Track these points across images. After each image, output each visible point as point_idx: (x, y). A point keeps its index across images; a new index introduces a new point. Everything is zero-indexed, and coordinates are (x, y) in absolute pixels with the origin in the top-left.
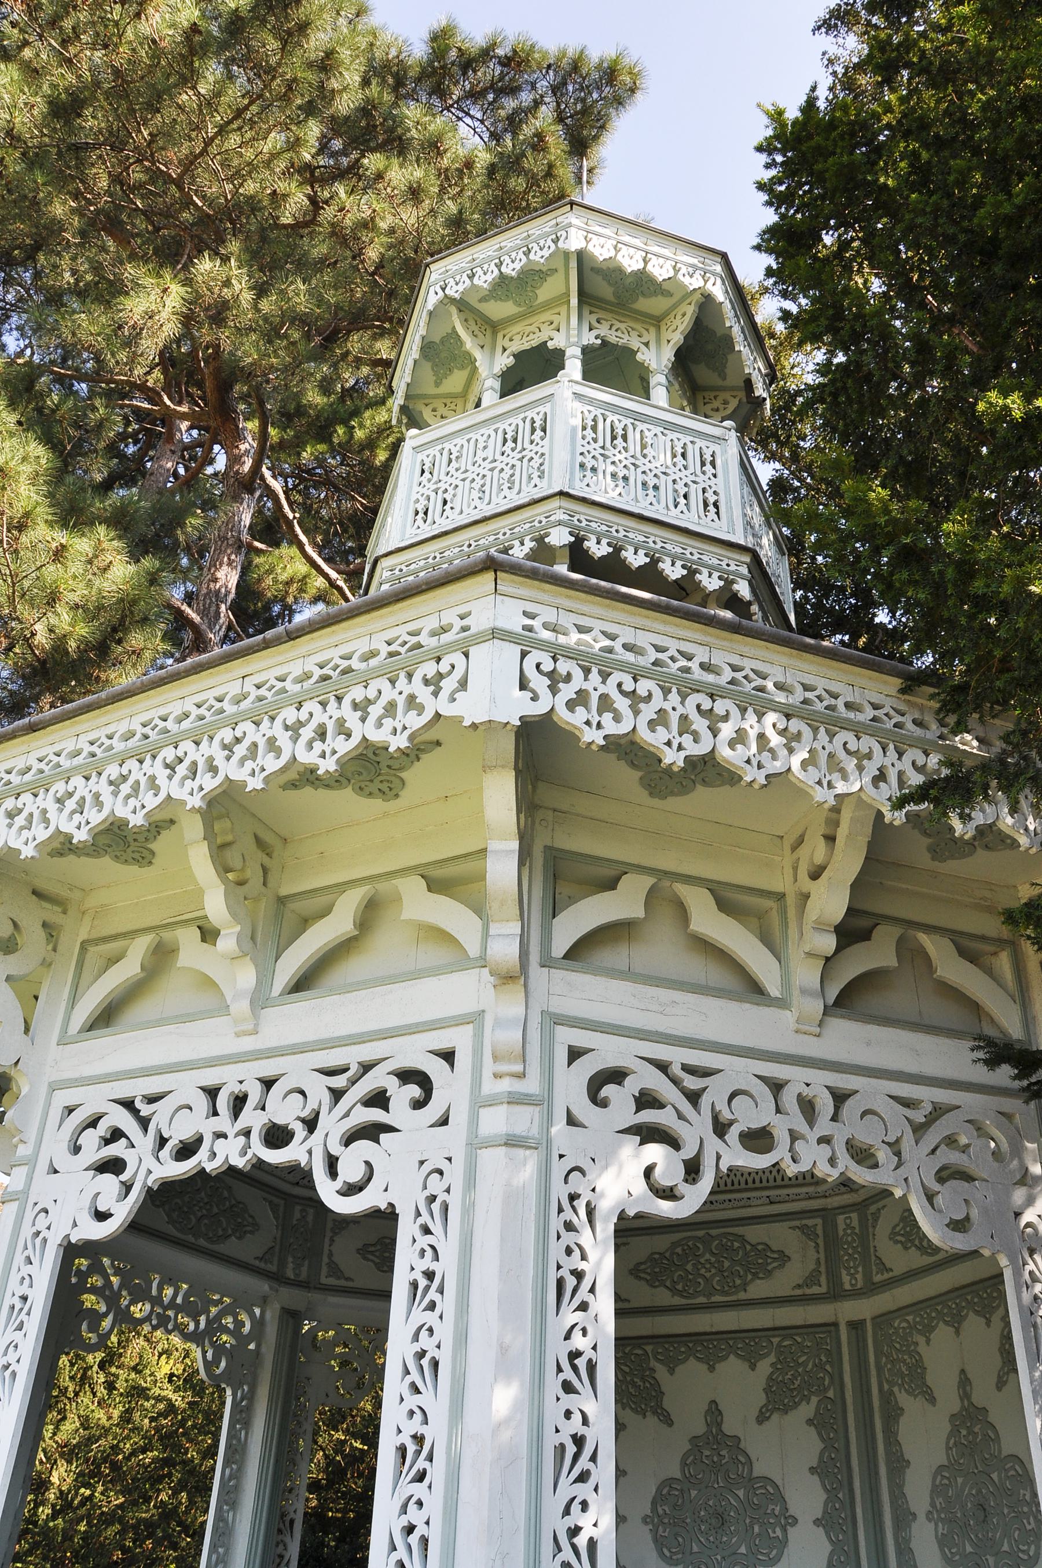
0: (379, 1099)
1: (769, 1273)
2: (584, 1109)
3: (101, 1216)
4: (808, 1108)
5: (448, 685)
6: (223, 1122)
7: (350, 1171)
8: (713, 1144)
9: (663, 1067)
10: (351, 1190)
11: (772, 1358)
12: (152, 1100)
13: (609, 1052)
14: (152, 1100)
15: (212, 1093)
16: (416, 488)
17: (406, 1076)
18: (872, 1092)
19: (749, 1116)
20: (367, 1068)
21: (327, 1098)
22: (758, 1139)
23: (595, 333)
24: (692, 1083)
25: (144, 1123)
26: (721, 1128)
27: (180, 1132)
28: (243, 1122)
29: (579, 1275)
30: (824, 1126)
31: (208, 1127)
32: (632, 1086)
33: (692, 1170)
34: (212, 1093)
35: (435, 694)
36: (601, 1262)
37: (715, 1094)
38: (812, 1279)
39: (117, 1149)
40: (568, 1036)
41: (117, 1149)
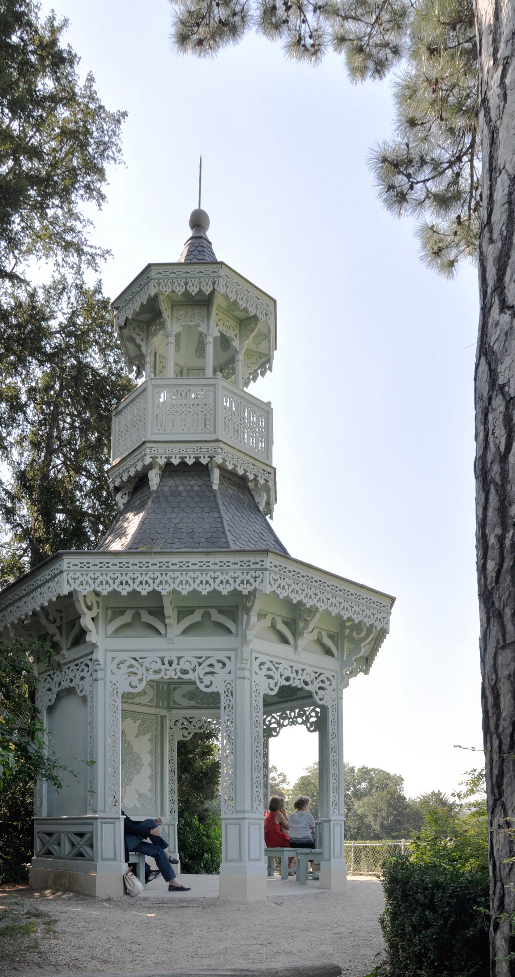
0: (211, 665)
1: (189, 692)
2: (115, 670)
4: (297, 672)
5: (259, 580)
11: (140, 721)
13: (121, 656)
17: (219, 661)
18: (309, 670)
19: (287, 674)
20: (207, 658)
22: (287, 679)
26: (148, 670)
30: (300, 676)
32: (127, 664)
33: (276, 684)
34: (162, 659)
35: (255, 581)
38: (175, 689)
40: (255, 655)
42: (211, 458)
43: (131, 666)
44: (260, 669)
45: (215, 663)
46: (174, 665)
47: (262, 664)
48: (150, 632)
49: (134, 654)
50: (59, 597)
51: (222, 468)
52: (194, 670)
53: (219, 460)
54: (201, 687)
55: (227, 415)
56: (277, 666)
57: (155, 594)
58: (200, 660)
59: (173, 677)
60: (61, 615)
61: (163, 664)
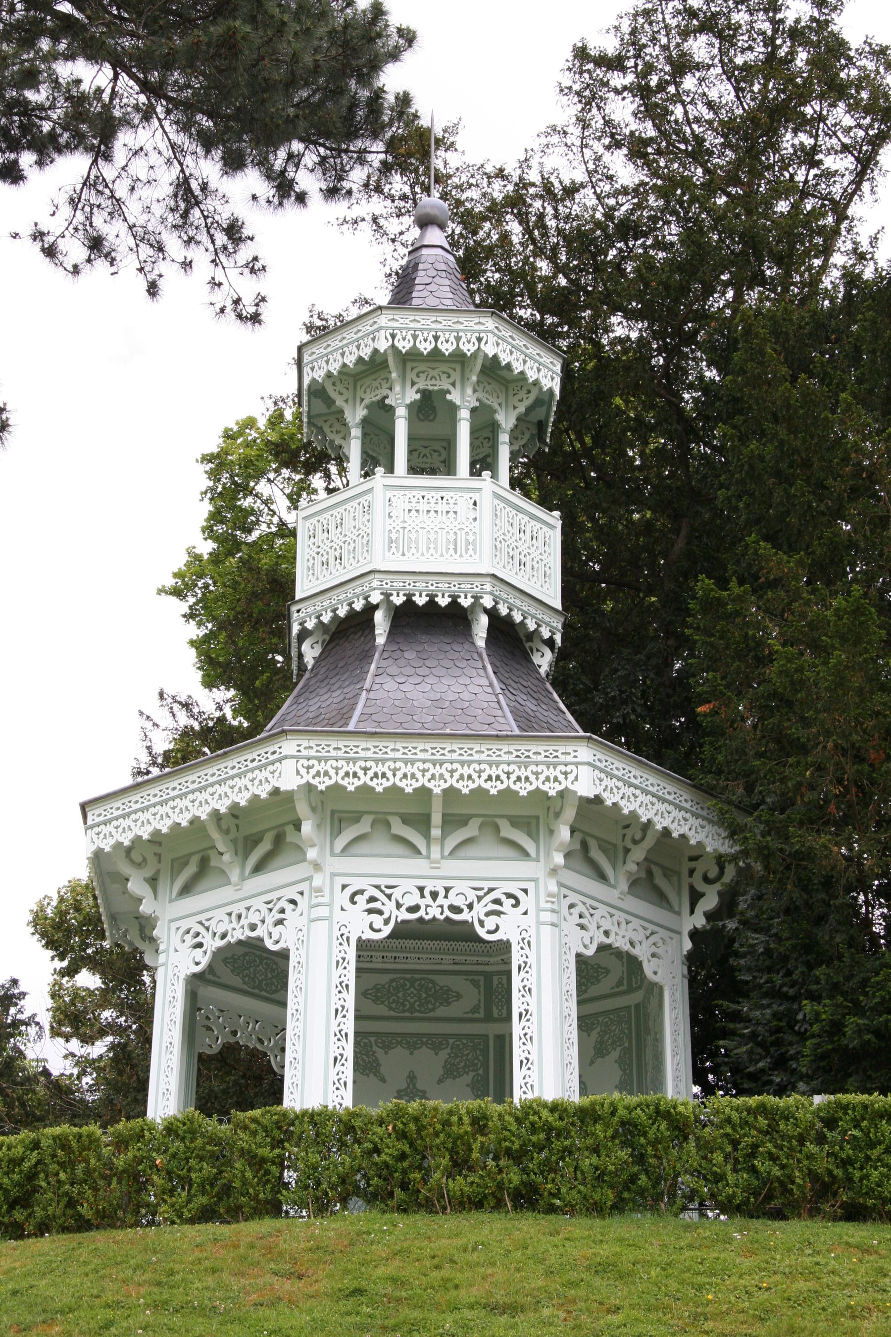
0: (497, 902)
2: (347, 905)
3: (197, 964)
4: (434, 895)
5: (571, 777)
6: (234, 924)
7: (275, 937)
8: (395, 912)
9: (377, 887)
10: (489, 932)
12: (208, 920)
13: (357, 884)
14: (208, 920)
15: (230, 914)
16: (477, 530)
17: (509, 896)
20: (491, 890)
21: (267, 911)
22: (414, 909)
23: (416, 388)
24: (388, 891)
25: (208, 929)
26: (399, 906)
27: (220, 930)
28: (241, 924)
29: (344, 959)
31: (230, 928)
32: (366, 895)
33: (387, 922)
34: (421, 889)
36: (352, 954)
37: (397, 894)
39: (199, 939)
41: (199, 939)
42: (477, 598)
43: (372, 899)
44: (571, 914)
45: (503, 898)
46: (440, 900)
47: (571, 906)
48: (399, 849)
49: (377, 881)
50: (276, 792)
51: (492, 613)
52: (470, 907)
53: (488, 602)
54: (482, 932)
55: (498, 534)
56: (592, 911)
57: (424, 793)
58: (481, 893)
59: (438, 916)
60: (236, 821)
61: (423, 896)
